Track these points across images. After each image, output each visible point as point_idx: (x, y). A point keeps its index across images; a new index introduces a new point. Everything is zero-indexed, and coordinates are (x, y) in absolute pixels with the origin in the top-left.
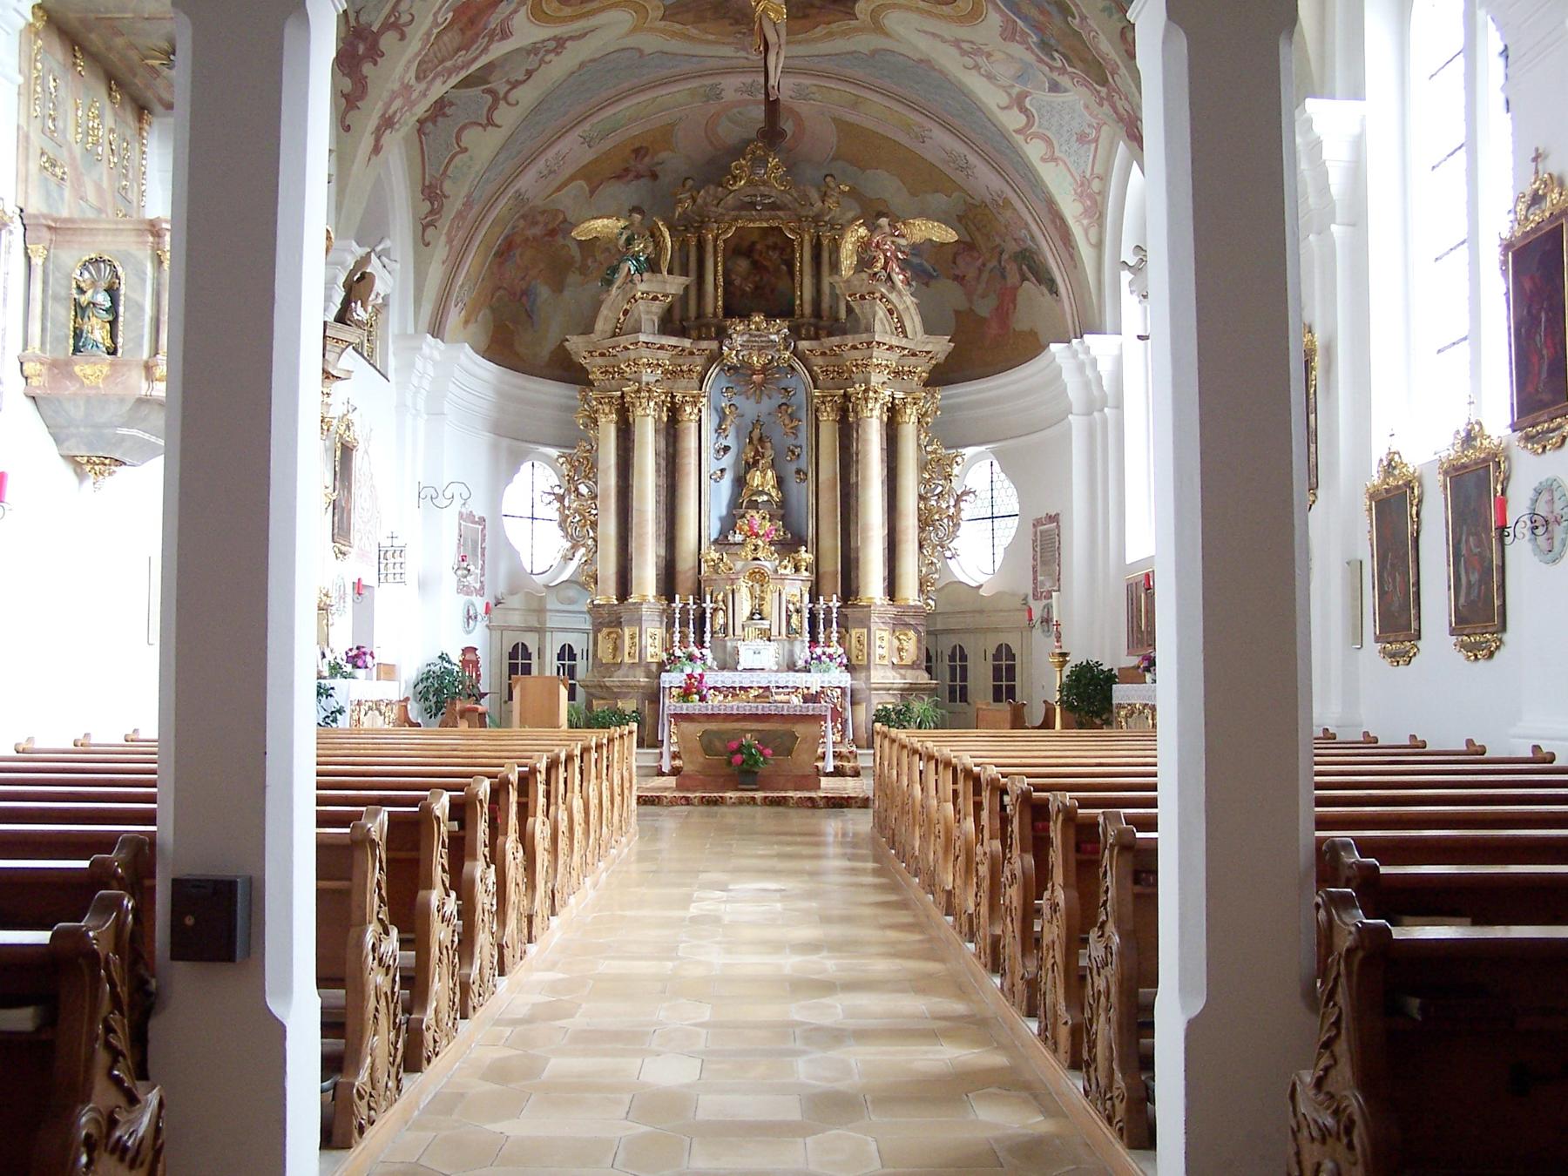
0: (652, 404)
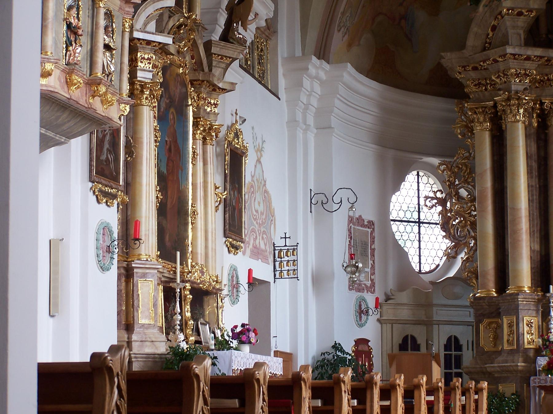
0: (521, 111)
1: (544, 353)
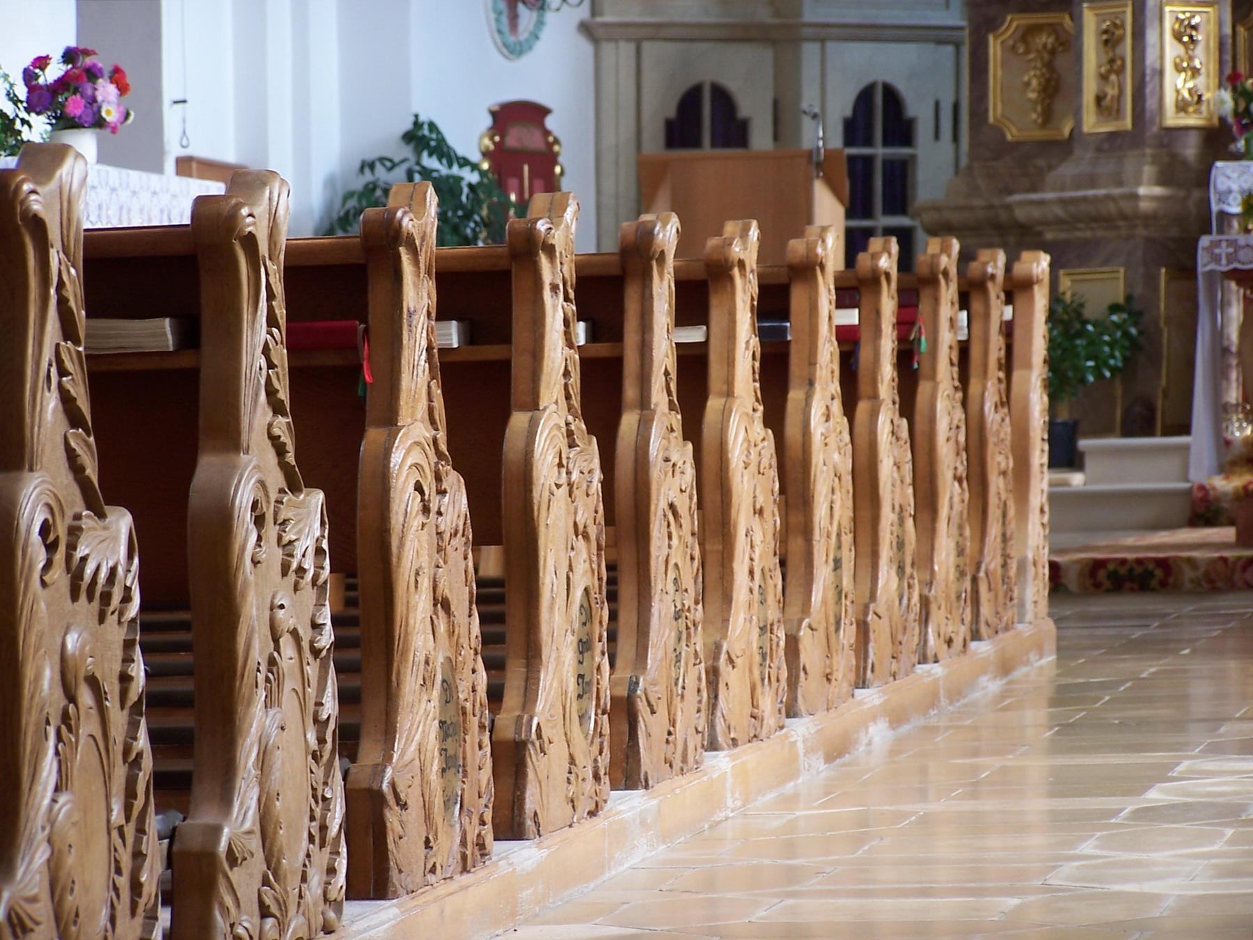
1: (1241, 144)
